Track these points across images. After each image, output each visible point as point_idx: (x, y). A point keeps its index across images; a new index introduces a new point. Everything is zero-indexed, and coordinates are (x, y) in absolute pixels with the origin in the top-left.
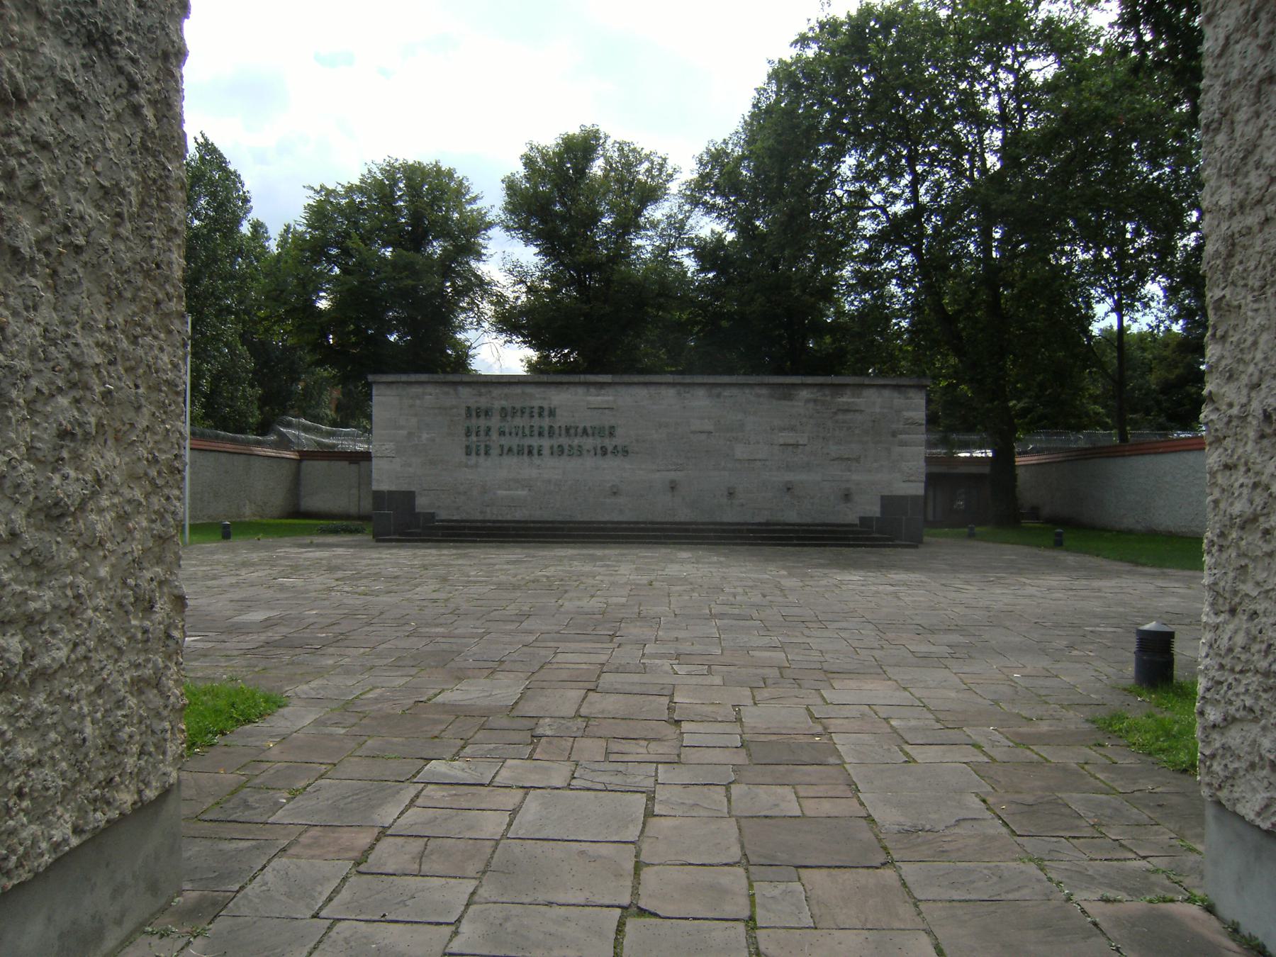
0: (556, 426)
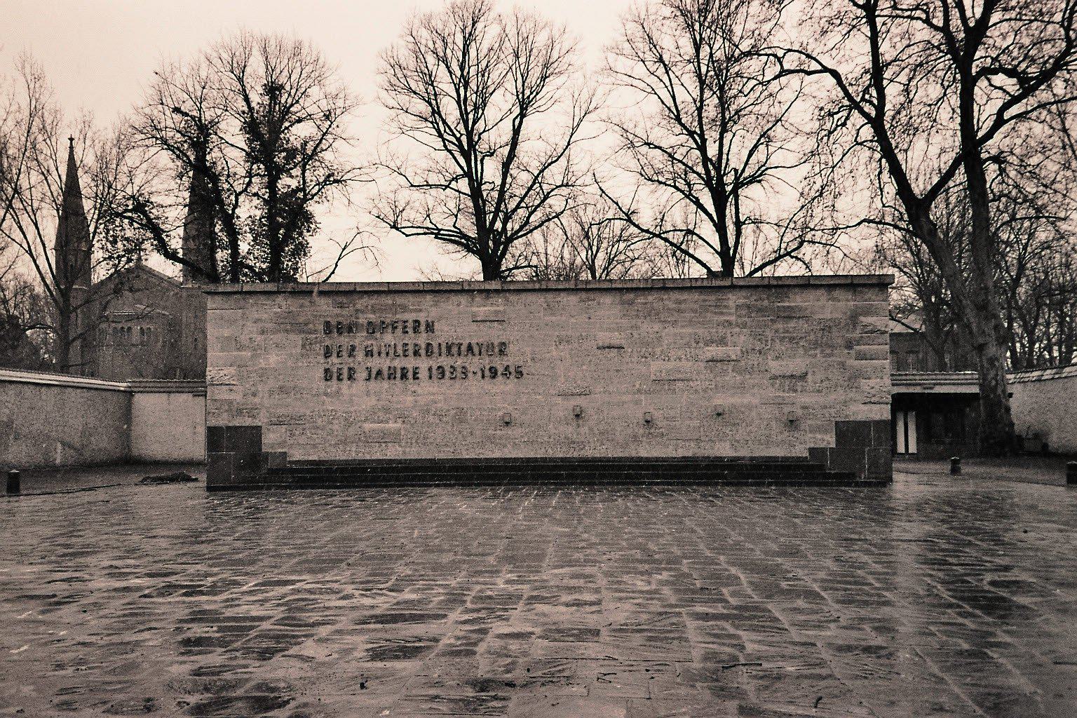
0: (435, 344)
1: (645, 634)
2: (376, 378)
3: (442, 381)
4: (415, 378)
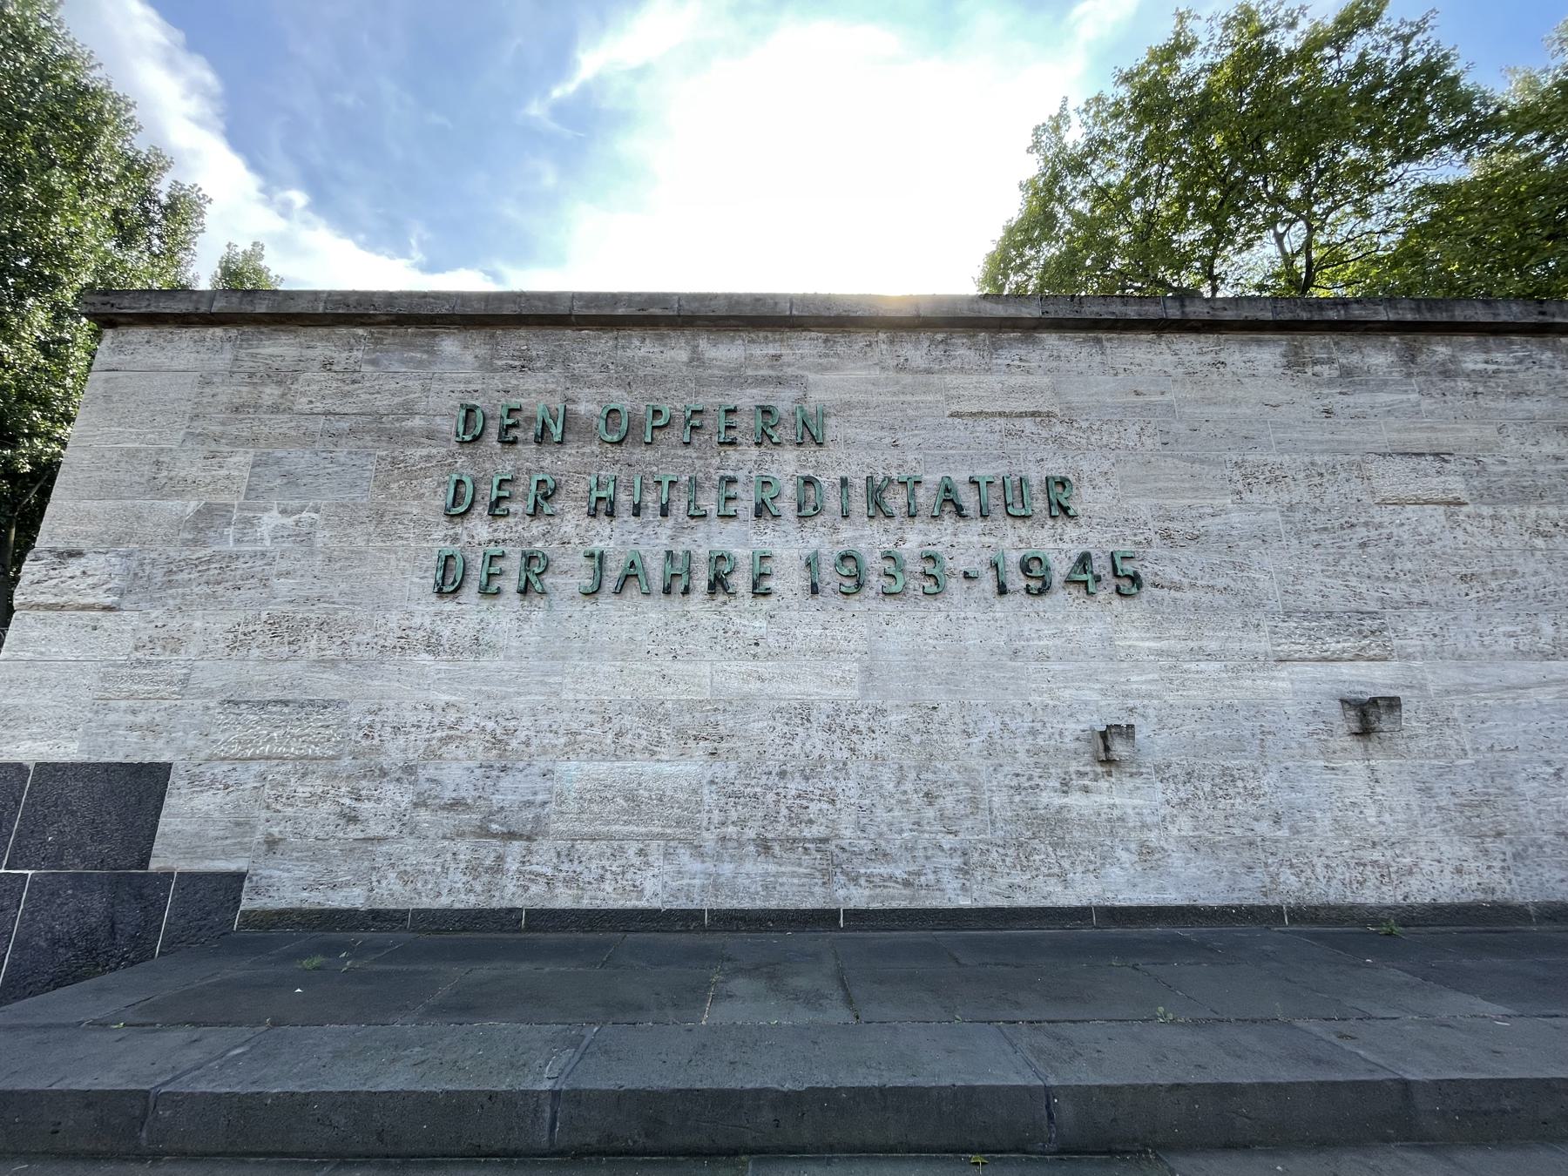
0: (828, 479)
1: (137, 1007)
2: (619, 591)
3: (854, 604)
4: (759, 590)
